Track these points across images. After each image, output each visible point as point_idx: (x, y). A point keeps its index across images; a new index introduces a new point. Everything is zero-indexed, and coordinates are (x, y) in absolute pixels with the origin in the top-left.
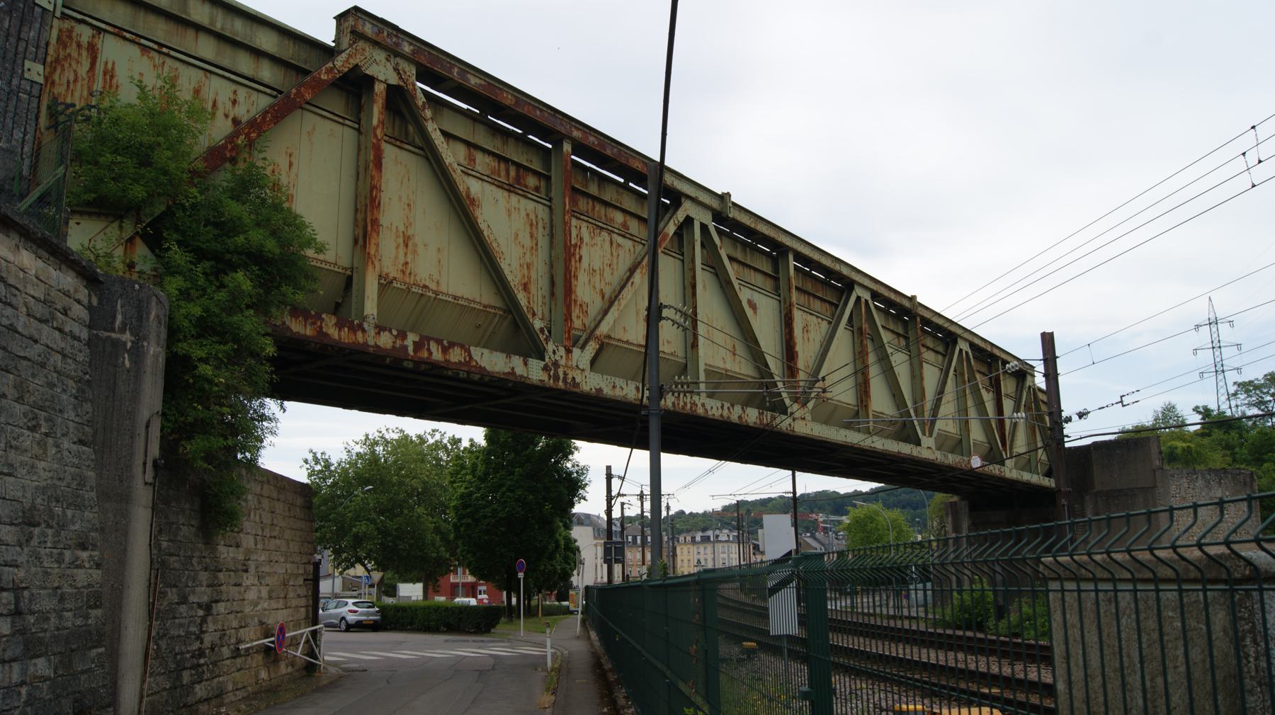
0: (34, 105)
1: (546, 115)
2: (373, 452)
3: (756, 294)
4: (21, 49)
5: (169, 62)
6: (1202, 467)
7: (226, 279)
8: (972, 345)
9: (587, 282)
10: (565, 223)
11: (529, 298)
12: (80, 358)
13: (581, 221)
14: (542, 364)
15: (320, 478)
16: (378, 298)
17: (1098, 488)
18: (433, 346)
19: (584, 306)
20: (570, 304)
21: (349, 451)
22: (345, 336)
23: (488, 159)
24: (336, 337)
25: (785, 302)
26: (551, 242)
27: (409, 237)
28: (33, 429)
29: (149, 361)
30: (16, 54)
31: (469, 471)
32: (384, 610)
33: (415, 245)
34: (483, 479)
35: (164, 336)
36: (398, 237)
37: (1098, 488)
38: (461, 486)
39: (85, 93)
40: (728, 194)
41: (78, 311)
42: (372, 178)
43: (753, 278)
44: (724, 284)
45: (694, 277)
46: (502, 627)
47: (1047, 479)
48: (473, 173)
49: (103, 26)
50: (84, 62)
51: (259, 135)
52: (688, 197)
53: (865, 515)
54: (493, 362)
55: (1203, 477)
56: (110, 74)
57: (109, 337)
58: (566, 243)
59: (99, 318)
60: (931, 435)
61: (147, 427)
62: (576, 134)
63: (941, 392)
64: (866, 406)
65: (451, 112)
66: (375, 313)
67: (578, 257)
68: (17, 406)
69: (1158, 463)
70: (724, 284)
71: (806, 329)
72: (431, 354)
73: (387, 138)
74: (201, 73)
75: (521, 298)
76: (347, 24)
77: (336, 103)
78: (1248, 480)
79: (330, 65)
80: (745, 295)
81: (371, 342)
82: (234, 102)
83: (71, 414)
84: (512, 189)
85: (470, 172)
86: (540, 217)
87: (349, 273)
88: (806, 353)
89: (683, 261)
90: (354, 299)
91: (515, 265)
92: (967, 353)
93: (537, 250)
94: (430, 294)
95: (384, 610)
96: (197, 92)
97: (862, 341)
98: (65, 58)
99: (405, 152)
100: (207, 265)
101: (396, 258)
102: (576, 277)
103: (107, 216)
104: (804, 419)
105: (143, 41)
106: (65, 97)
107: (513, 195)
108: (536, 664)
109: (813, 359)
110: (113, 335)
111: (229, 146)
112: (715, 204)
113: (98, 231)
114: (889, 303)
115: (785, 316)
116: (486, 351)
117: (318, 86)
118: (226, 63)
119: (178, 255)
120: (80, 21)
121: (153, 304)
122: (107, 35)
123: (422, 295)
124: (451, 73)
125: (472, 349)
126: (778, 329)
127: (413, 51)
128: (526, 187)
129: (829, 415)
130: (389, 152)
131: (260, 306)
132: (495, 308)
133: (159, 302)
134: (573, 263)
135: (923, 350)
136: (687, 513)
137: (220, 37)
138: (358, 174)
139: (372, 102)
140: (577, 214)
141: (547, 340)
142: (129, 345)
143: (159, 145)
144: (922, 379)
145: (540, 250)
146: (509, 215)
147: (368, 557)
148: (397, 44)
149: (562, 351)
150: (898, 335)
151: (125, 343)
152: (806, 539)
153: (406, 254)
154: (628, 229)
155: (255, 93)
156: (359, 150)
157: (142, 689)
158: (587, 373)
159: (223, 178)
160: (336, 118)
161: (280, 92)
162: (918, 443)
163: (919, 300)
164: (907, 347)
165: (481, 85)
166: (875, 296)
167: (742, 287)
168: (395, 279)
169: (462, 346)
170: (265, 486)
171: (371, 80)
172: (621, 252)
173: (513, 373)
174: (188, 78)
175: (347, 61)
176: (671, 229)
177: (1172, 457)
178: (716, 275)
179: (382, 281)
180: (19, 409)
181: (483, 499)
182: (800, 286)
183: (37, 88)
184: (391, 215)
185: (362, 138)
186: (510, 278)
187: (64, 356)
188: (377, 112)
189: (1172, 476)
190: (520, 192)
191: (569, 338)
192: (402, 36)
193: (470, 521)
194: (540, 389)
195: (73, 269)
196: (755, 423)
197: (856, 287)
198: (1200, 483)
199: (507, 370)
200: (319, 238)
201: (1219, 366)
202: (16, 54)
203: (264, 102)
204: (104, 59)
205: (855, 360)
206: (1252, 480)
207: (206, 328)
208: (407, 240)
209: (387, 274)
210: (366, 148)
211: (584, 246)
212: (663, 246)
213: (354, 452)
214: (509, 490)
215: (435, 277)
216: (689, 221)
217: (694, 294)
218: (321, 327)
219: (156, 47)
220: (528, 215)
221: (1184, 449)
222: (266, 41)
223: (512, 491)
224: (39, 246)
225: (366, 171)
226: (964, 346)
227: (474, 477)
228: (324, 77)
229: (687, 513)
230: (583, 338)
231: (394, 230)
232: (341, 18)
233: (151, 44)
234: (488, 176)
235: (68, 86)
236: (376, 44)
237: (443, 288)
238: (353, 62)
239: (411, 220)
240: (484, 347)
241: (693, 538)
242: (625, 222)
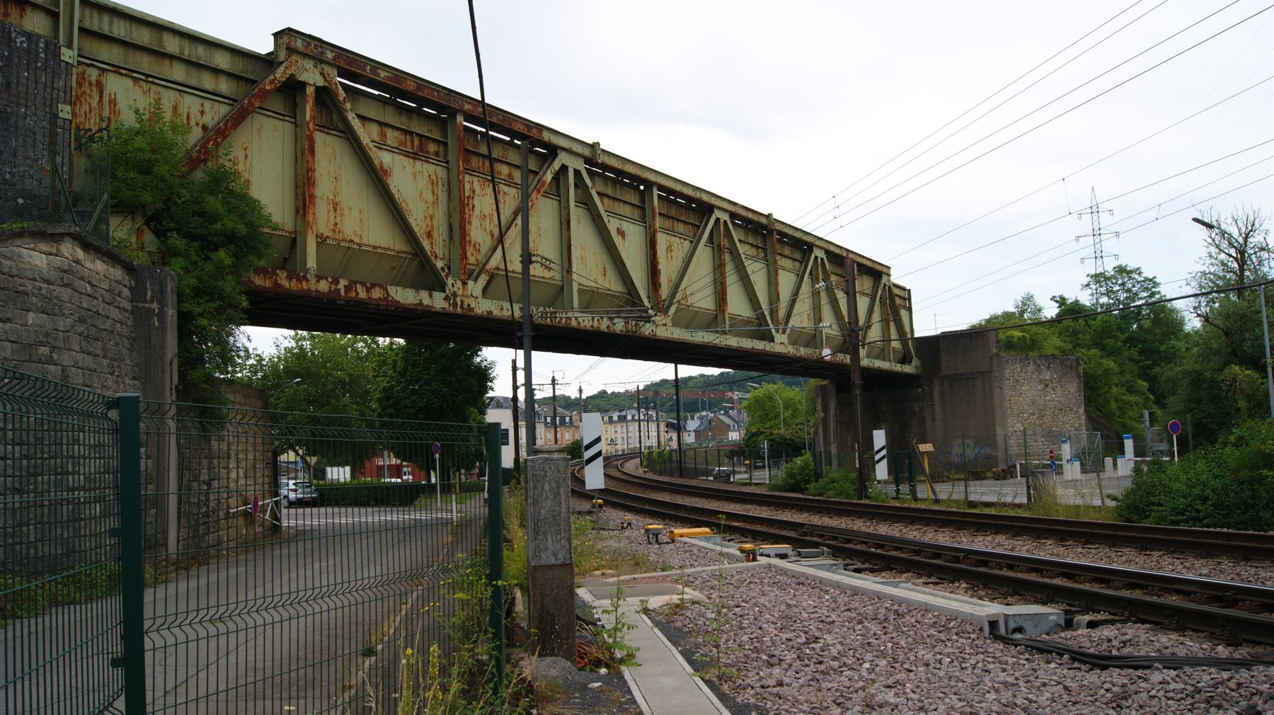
0: (67, 136)
1: (442, 94)
2: (301, 348)
3: (625, 224)
4: (54, 96)
5: (154, 87)
6: (1036, 354)
7: (214, 256)
8: (827, 252)
9: (479, 225)
10: (460, 182)
11: (432, 244)
12: (129, 324)
13: (472, 177)
14: (444, 295)
15: (250, 372)
16: (317, 251)
17: (945, 372)
18: (359, 288)
19: (477, 245)
20: (465, 246)
21: (278, 346)
22: (293, 285)
23: (396, 134)
24: (288, 286)
25: (650, 228)
26: (449, 196)
27: (337, 204)
28: (112, 374)
29: (169, 320)
30: (52, 100)
31: (390, 367)
32: (320, 490)
33: (342, 209)
34: (402, 374)
35: (175, 301)
36: (328, 204)
37: (945, 372)
38: (384, 381)
39: (98, 120)
40: (598, 144)
41: (126, 292)
42: (308, 162)
43: (622, 209)
44: (595, 218)
45: (569, 215)
46: (422, 500)
47: (899, 365)
48: (385, 147)
49: (105, 67)
50: (95, 96)
51: (223, 140)
52: (563, 149)
53: (765, 395)
54: (405, 296)
55: (1035, 362)
56: (113, 102)
57: (144, 307)
58: (460, 198)
59: (137, 294)
60: (784, 332)
61: (171, 364)
62: (467, 107)
63: (796, 294)
64: (723, 311)
65: (365, 98)
66: (315, 266)
67: (471, 206)
68: (105, 361)
69: (995, 351)
70: (595, 218)
71: (669, 249)
72: (357, 293)
73: (317, 127)
74: (177, 93)
75: (426, 245)
76: (282, 41)
77: (277, 104)
78: (1074, 364)
79: (272, 77)
80: (613, 225)
81: (313, 288)
82: (202, 113)
83: (128, 361)
84: (416, 157)
85: (383, 146)
86: (439, 177)
87: (293, 235)
88: (668, 269)
89: (560, 201)
90: (298, 251)
91: (421, 217)
92: (822, 259)
93: (437, 203)
94: (355, 246)
95: (320, 490)
96: (175, 108)
97: (720, 256)
98: (82, 96)
99: (330, 136)
100: (197, 244)
101: (328, 220)
102: (470, 223)
103: (123, 212)
104: (665, 325)
105: (134, 75)
106: (85, 124)
107: (417, 161)
108: (446, 523)
109: (676, 272)
110: (146, 305)
111: (203, 151)
112: (587, 152)
113: (117, 225)
114: (747, 221)
115: (650, 240)
116: (399, 289)
117: (264, 94)
118: (194, 82)
119: (176, 241)
120: (89, 65)
121: (169, 280)
122: (109, 73)
123: (349, 248)
124: (365, 70)
125: (389, 287)
126: (644, 251)
127: (334, 57)
128: (428, 152)
129: (689, 318)
130: (319, 137)
131: (235, 270)
132: (406, 253)
133: (172, 278)
134: (467, 211)
135: (778, 257)
136: (609, 393)
137: (188, 63)
138: (296, 158)
139: (305, 102)
140: (469, 171)
141: (447, 276)
142: (157, 310)
143: (157, 161)
144: (777, 285)
145: (440, 203)
146: (415, 178)
147: (299, 443)
148: (322, 53)
149: (459, 284)
150: (757, 247)
151: (154, 310)
152: (720, 417)
153: (335, 217)
154: (513, 179)
155: (217, 104)
156: (296, 140)
157: (178, 536)
158: (480, 299)
159: (199, 175)
160: (278, 116)
161: (235, 101)
162: (772, 340)
163: (775, 216)
164: (766, 259)
165: (389, 77)
166: (733, 216)
167: (611, 219)
168: (328, 237)
169: (381, 286)
170: (237, 395)
171: (303, 85)
172: (507, 199)
173: (421, 303)
174: (169, 98)
175: (284, 72)
176: (549, 177)
177: (1010, 345)
178: (589, 210)
179: (319, 240)
180: (105, 362)
181: (403, 392)
182: (664, 212)
183: (68, 123)
184: (323, 189)
185: (298, 129)
186: (416, 230)
187: (121, 323)
188: (309, 110)
189: (1007, 362)
190: (423, 158)
191: (465, 273)
192: (326, 46)
193: (392, 411)
194: (443, 314)
195: (121, 265)
196: (621, 331)
197: (715, 210)
198: (1031, 367)
199: (417, 302)
200: (274, 219)
201: (1098, 252)
202: (52, 100)
203: (223, 110)
204: (108, 92)
205: (714, 270)
206: (1078, 364)
207: (199, 292)
208: (336, 206)
209: (322, 234)
210: (302, 137)
211: (476, 197)
212: (544, 189)
213: (282, 347)
214: (426, 383)
215: (359, 232)
216: (564, 168)
217: (569, 229)
218: (276, 280)
219: (144, 78)
220: (430, 176)
221: (1019, 338)
222: (222, 61)
223: (429, 385)
224: (104, 255)
225: (302, 155)
226: (819, 253)
227: (395, 372)
228: (268, 87)
229: (609, 393)
230: (477, 271)
231: (325, 198)
232: (278, 35)
233: (140, 76)
234: (397, 149)
235: (86, 116)
236: (305, 56)
237: (365, 241)
238: (289, 72)
239: (338, 189)
240: (396, 285)
241: (611, 418)
242: (510, 173)
